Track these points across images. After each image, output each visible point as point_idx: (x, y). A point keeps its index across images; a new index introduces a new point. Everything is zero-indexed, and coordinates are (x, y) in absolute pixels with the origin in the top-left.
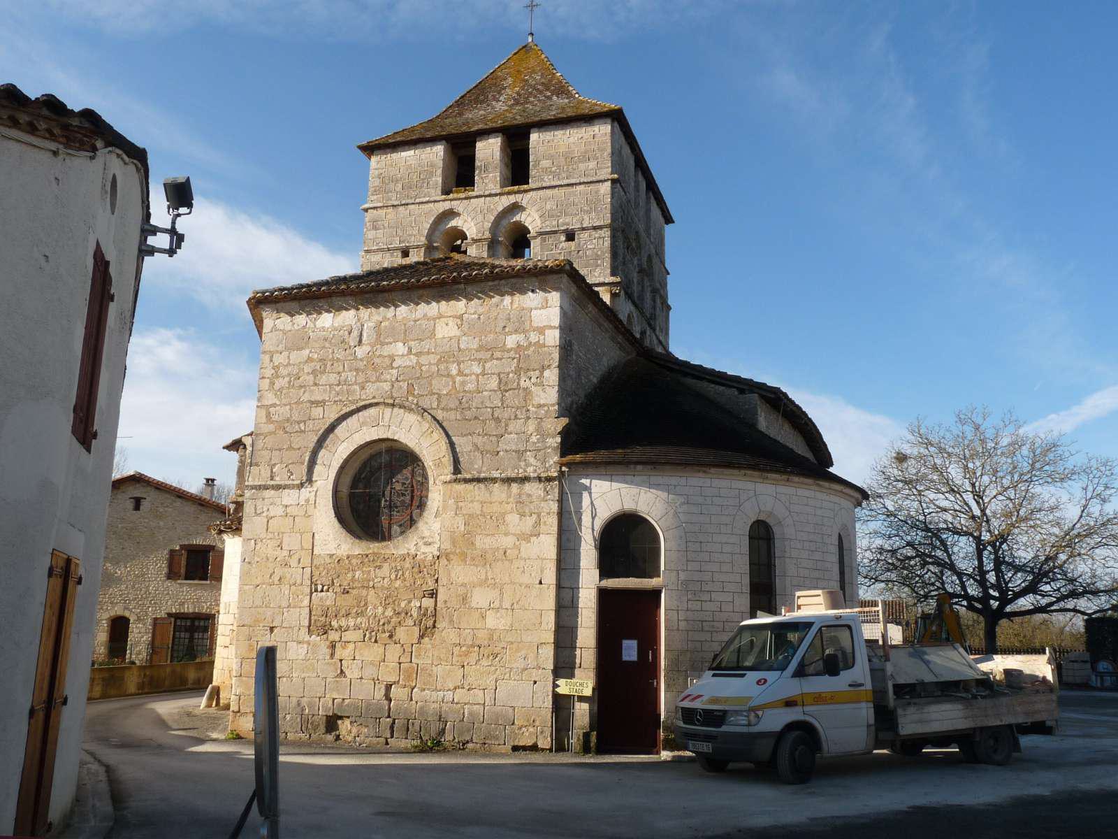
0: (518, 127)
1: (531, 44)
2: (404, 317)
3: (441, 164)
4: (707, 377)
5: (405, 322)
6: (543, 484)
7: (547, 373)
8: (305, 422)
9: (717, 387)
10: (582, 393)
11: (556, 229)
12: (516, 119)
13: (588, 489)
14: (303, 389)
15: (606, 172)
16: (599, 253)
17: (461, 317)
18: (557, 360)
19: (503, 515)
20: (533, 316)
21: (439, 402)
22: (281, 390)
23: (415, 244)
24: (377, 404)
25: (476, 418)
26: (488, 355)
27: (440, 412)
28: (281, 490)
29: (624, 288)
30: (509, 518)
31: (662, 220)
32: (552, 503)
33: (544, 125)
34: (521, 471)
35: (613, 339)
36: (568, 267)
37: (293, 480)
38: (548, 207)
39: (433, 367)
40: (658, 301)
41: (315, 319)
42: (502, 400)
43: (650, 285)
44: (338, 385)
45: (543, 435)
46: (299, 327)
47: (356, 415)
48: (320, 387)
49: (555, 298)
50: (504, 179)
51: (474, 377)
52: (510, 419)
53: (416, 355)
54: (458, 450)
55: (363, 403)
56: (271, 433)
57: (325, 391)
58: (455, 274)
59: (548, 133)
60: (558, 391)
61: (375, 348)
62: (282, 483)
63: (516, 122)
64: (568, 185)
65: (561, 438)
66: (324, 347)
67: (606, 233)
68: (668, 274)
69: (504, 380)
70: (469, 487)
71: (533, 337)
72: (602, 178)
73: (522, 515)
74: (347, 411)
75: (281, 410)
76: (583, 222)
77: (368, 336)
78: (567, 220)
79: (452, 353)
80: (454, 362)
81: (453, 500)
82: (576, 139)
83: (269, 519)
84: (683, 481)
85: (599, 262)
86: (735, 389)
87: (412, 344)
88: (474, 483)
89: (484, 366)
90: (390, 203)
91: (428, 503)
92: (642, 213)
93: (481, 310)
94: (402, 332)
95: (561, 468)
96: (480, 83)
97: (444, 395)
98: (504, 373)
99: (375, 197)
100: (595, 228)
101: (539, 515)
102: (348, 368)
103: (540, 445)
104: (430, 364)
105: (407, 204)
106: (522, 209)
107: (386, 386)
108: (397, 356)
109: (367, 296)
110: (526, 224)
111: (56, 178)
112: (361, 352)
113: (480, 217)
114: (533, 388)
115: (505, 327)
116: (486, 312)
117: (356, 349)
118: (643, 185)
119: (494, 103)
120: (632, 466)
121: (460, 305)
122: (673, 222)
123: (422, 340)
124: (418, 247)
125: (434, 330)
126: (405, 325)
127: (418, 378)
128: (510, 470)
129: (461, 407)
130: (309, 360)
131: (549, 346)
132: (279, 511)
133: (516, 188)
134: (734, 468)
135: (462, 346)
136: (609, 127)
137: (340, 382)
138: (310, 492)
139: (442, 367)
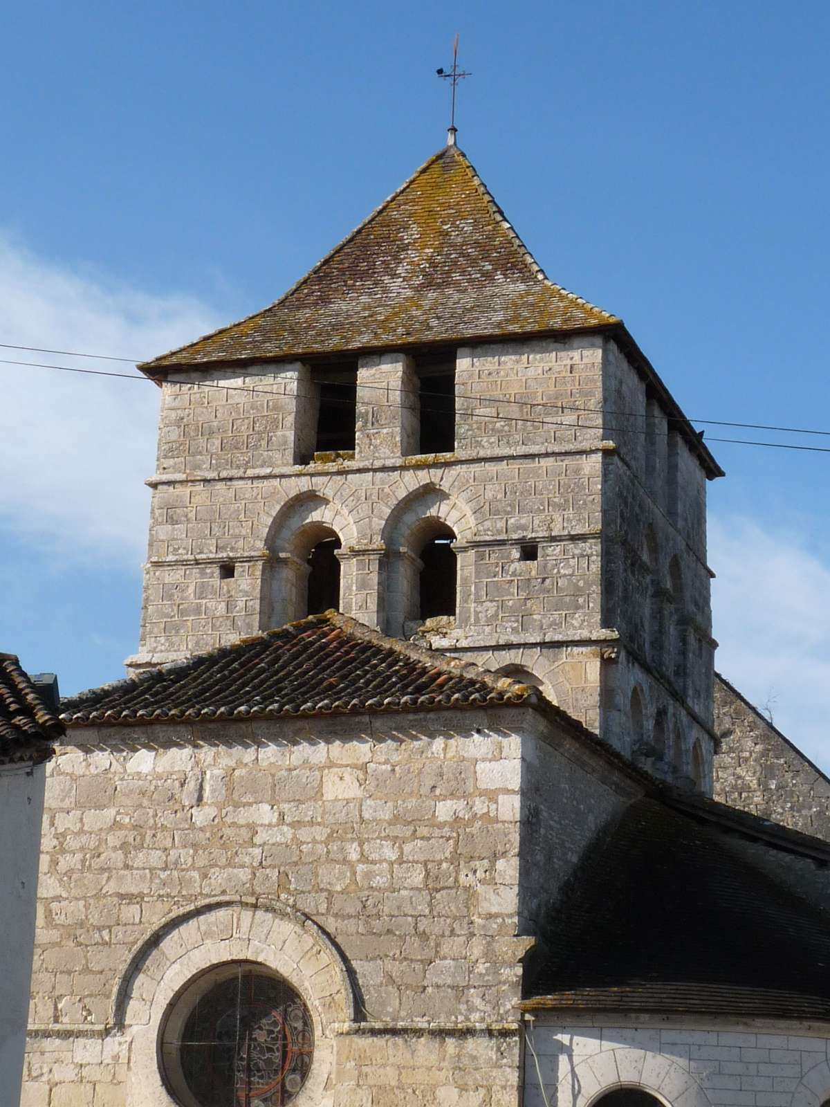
0: (432, 345)
1: (452, 151)
2: (271, 764)
3: (292, 405)
4: (764, 837)
5: (273, 772)
6: (494, 1040)
7: (501, 864)
8: (110, 927)
9: (781, 855)
10: (554, 886)
11: (503, 537)
12: (430, 328)
13: (569, 1051)
14: (106, 874)
15: (593, 437)
16: (581, 583)
17: (364, 768)
18: (517, 844)
19: (433, 1088)
20: (479, 772)
21: (330, 903)
22: (69, 873)
23: (246, 554)
24: (228, 904)
25: (389, 932)
26: (407, 830)
27: (331, 920)
28: (71, 1039)
29: (625, 647)
30: (441, 1093)
31: (699, 474)
32: (508, 1070)
33: (480, 344)
34: (460, 1018)
35: (604, 780)
36: (534, 700)
37: (92, 1023)
38: (489, 495)
39: (318, 846)
40: (692, 639)
41: (125, 759)
42: (430, 905)
43: (677, 610)
44: (164, 869)
45: (495, 963)
46: (98, 770)
47: (195, 919)
48: (135, 872)
49: (513, 745)
50: (408, 436)
51: (385, 865)
52: (443, 936)
53: (291, 825)
54: (360, 982)
55: (207, 901)
56: (54, 944)
57: (143, 878)
58: (355, 701)
59: (490, 359)
60: (518, 894)
61: (224, 811)
62: (75, 1027)
63: (429, 336)
64: (525, 456)
65: (523, 967)
66: (140, 806)
67: (594, 548)
68: (713, 576)
69: (434, 872)
70: (379, 1041)
71: (480, 806)
72: (586, 445)
73: (463, 1089)
74: (181, 913)
75: (71, 907)
76: (552, 525)
77: (213, 791)
78: (523, 521)
79: (350, 825)
80: (353, 840)
81: (353, 1064)
82: (540, 371)
83: (52, 1086)
84: (712, 1038)
85: (581, 600)
86: (809, 860)
87: (285, 807)
88: (388, 1036)
89: (401, 848)
90: (199, 474)
91: (313, 1067)
92: (659, 483)
93: (395, 758)
94: (269, 786)
95: (523, 1015)
96: (359, 232)
97: (338, 893)
98: (433, 861)
99: (171, 462)
100: (573, 538)
101: (489, 1090)
102: (179, 841)
103: (490, 978)
104: (314, 841)
105: (231, 479)
106: (441, 495)
107: (244, 875)
108: (262, 825)
109: (212, 726)
110: (448, 523)
111: (29, 798)
112: (201, 816)
113: (365, 509)
114: (480, 889)
115: (434, 787)
116: (405, 762)
117: (193, 810)
118: (662, 426)
119: (386, 279)
120: (633, 1015)
121: (361, 749)
122: (722, 474)
123: (300, 802)
124: (250, 559)
125: (321, 785)
126: (273, 776)
127: (296, 864)
128: (443, 1015)
129: (365, 913)
130: (116, 825)
131: (504, 822)
132: (69, 1073)
133: (430, 457)
134: (791, 1018)
135: (366, 816)
136: (599, 352)
137: (167, 866)
138: (120, 1044)
139: (334, 847)
